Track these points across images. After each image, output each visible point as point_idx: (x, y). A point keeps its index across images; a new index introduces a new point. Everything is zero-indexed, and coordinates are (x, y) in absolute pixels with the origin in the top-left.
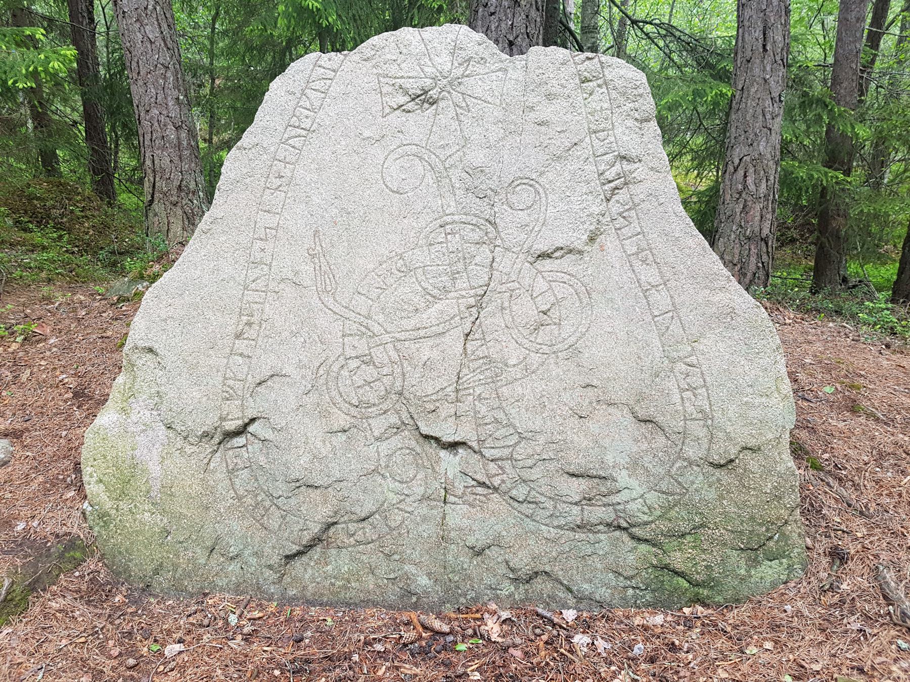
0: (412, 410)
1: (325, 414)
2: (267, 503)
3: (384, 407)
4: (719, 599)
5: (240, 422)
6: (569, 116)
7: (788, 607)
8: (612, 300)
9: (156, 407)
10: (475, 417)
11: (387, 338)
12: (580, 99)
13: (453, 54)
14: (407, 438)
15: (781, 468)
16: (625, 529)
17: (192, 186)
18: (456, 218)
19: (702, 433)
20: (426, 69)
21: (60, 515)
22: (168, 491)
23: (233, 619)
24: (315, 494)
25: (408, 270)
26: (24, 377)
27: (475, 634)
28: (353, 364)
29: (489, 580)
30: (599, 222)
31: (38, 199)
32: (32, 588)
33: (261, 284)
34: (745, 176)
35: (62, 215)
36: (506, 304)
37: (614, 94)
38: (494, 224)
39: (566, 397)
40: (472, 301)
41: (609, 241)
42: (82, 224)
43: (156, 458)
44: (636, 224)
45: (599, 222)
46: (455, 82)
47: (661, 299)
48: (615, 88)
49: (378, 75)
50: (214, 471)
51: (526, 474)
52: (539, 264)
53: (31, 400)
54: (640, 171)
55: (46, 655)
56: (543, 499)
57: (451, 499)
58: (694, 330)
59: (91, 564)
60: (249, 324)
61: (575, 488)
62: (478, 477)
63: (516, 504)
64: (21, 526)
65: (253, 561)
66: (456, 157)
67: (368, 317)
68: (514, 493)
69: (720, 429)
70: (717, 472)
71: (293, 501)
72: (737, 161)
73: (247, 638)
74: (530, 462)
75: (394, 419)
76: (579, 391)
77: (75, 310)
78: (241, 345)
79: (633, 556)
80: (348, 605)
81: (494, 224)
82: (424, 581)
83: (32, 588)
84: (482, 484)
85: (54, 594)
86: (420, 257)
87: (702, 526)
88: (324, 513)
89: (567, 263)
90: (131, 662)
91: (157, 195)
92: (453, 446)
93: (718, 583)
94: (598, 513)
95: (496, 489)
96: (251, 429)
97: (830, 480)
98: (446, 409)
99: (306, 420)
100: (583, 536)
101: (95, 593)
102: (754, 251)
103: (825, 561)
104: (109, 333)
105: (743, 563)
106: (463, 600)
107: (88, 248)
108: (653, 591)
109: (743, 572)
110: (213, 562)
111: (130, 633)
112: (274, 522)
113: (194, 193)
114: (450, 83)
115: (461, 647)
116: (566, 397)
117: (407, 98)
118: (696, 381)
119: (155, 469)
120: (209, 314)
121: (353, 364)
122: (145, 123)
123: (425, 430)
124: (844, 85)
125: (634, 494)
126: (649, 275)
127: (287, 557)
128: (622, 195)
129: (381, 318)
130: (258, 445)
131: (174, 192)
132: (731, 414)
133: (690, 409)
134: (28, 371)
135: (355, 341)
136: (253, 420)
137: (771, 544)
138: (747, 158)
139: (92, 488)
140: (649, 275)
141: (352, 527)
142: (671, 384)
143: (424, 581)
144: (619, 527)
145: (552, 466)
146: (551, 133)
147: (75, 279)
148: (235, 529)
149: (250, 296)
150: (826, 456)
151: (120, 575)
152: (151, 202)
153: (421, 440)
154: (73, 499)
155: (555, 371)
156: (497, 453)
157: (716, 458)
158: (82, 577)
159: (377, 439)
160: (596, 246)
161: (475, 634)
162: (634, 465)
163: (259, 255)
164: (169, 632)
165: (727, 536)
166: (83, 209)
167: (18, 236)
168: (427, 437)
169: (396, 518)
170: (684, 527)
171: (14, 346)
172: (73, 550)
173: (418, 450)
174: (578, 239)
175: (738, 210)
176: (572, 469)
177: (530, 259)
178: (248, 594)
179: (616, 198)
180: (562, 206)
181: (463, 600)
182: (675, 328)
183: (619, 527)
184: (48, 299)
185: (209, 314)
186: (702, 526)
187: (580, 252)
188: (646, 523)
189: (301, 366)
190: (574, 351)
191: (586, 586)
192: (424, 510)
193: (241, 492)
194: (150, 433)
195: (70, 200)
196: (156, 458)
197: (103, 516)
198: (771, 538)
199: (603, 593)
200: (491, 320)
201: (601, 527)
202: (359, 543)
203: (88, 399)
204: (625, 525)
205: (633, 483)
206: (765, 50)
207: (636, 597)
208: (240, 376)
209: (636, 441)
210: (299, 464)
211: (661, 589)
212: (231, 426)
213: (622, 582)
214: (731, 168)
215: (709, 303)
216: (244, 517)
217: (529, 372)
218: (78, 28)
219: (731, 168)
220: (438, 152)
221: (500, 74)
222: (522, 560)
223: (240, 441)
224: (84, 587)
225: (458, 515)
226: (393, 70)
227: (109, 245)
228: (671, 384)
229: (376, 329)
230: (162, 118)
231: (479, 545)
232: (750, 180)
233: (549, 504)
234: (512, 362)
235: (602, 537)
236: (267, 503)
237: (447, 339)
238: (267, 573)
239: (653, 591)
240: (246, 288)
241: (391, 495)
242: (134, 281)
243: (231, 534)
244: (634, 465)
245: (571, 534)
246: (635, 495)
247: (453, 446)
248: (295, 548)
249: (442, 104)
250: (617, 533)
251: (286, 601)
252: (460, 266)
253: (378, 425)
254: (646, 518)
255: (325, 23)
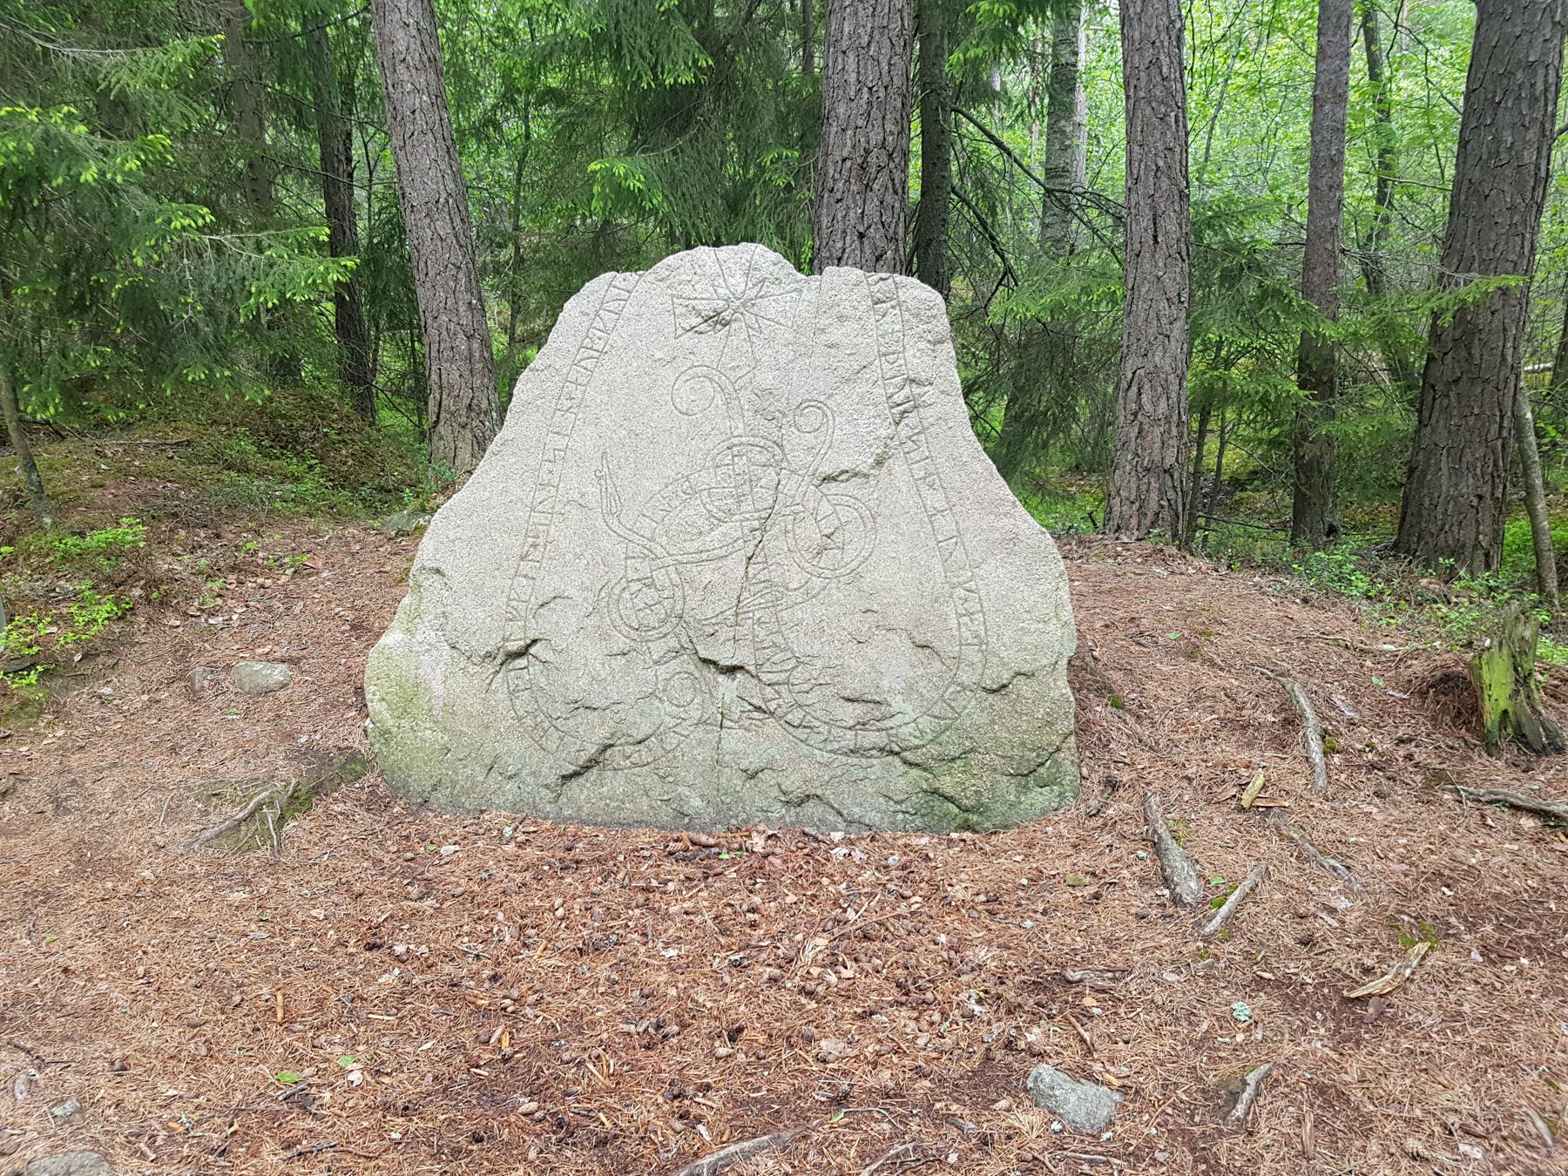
0: (691, 633)
1: (605, 637)
2: (546, 725)
3: (664, 630)
4: (987, 824)
5: (522, 643)
6: (860, 339)
7: (1050, 829)
8: (897, 525)
9: (441, 628)
10: (753, 641)
11: (669, 560)
12: (872, 321)
13: (747, 275)
14: (686, 663)
15: (1055, 694)
16: (897, 754)
17: (484, 405)
18: (743, 439)
19: (977, 658)
20: (720, 290)
21: (342, 732)
22: (450, 710)
23: (508, 831)
24: (592, 716)
25: (694, 492)
26: (297, 610)
27: (740, 849)
28: (635, 587)
29: (761, 802)
30: (886, 445)
31: (283, 417)
32: (316, 791)
33: (547, 506)
34: (1140, 394)
35: (314, 439)
36: (790, 527)
37: (907, 316)
38: (781, 447)
39: (845, 622)
40: (756, 524)
41: (897, 465)
42: (338, 451)
43: (439, 678)
44: (924, 448)
45: (886, 445)
46: (748, 304)
47: (946, 524)
48: (908, 310)
49: (672, 296)
50: (496, 692)
51: (801, 699)
52: (824, 488)
53: (306, 631)
54: (930, 394)
55: (330, 845)
56: (817, 724)
57: (727, 723)
58: (977, 556)
59: (370, 778)
60: (534, 546)
61: (851, 713)
62: (754, 701)
63: (791, 729)
64: (304, 739)
65: (530, 780)
66: (745, 379)
67: (652, 540)
68: (789, 716)
69: (996, 655)
70: (990, 697)
71: (571, 722)
72: (1130, 376)
73: (520, 846)
74: (806, 687)
75: (673, 643)
76: (859, 617)
77: (347, 544)
78: (525, 567)
79: (903, 780)
80: (622, 825)
81: (781, 447)
82: (696, 802)
83: (316, 791)
84: (758, 709)
85: (336, 800)
86: (706, 478)
87: (972, 750)
88: (600, 735)
89: (852, 486)
90: (409, 855)
91: (443, 415)
92: (732, 670)
93: (987, 809)
94: (871, 738)
95: (772, 714)
96: (532, 650)
97: (1128, 717)
98: (725, 633)
99: (587, 642)
100: (856, 761)
101: (375, 803)
102: (1154, 485)
103: (1097, 789)
104: (388, 568)
105: (1012, 788)
106: (733, 821)
107: (342, 481)
108: (923, 816)
109: (1012, 798)
110: (490, 781)
111: (407, 838)
112: (552, 744)
113: (486, 413)
114: (744, 304)
115: (725, 856)
116: (845, 622)
117: (700, 320)
118: (973, 606)
119: (438, 688)
120: (496, 536)
121: (635, 587)
122: (432, 331)
123: (703, 654)
124: (1318, 271)
125: (907, 719)
126: (935, 500)
127: (564, 777)
128: (912, 419)
129: (664, 540)
130: (539, 667)
131: (464, 412)
132: (1006, 639)
133: (967, 634)
134: (301, 603)
135: (637, 563)
136: (534, 641)
137: (1042, 770)
138: (1141, 372)
139: (374, 705)
140: (935, 500)
141: (628, 749)
142: (949, 610)
143: (696, 802)
144: (892, 752)
145: (828, 691)
146: (841, 356)
147: (336, 515)
148: (514, 749)
149: (537, 518)
150: (1133, 696)
151: (398, 790)
152: (437, 422)
153: (700, 664)
154: (354, 718)
155: (836, 595)
156: (774, 678)
157: (989, 683)
158: (362, 788)
159: (656, 663)
160: (884, 469)
161: (740, 849)
162: (910, 690)
163: (546, 477)
164: (445, 836)
165: (998, 762)
166: (340, 432)
167: (264, 464)
168: (705, 661)
169: (672, 741)
170: (954, 751)
171: (284, 579)
172: (353, 764)
173: (697, 674)
174: (864, 462)
175: (1133, 435)
176: (847, 693)
177: (816, 482)
178: (523, 813)
179: (906, 421)
180: (848, 429)
181: (733, 821)
182: (959, 554)
183: (892, 752)
184: (315, 533)
185: (496, 536)
186: (972, 750)
187: (866, 476)
188: (917, 747)
189: (583, 588)
190: (855, 576)
191: (856, 810)
192: (700, 733)
193: (520, 713)
194: (434, 652)
195: (323, 418)
196: (440, 677)
197: (385, 734)
198: (1042, 764)
199: (873, 817)
200: (775, 543)
201: (874, 752)
202: (635, 765)
203: (365, 630)
204: (897, 749)
205: (908, 708)
206: (1156, 241)
207: (905, 821)
208: (524, 598)
209: (913, 666)
210: (578, 685)
211: (931, 813)
212: (513, 646)
213: (892, 807)
214: (1124, 385)
215: (992, 529)
216: (523, 738)
217: (810, 596)
218: (242, 4)
219: (1124, 385)
220: (728, 373)
221: (794, 295)
222: (793, 784)
223: (522, 662)
224: (364, 797)
225: (733, 740)
226: (687, 290)
227: (372, 479)
228: (949, 610)
229: (659, 551)
230: (452, 326)
231: (752, 768)
232: (1144, 398)
233: (824, 729)
234: (792, 586)
235: (875, 762)
236: (546, 725)
237: (729, 562)
238: (544, 792)
239: (923, 816)
240: (533, 510)
241: (668, 719)
242: (414, 513)
243: (509, 752)
244: (910, 690)
245: (844, 759)
246: (909, 720)
247: (732, 670)
248: (572, 769)
249: (734, 325)
250: (890, 758)
251: (560, 820)
252: (747, 488)
253: (658, 649)
254: (917, 742)
255: (648, 206)
